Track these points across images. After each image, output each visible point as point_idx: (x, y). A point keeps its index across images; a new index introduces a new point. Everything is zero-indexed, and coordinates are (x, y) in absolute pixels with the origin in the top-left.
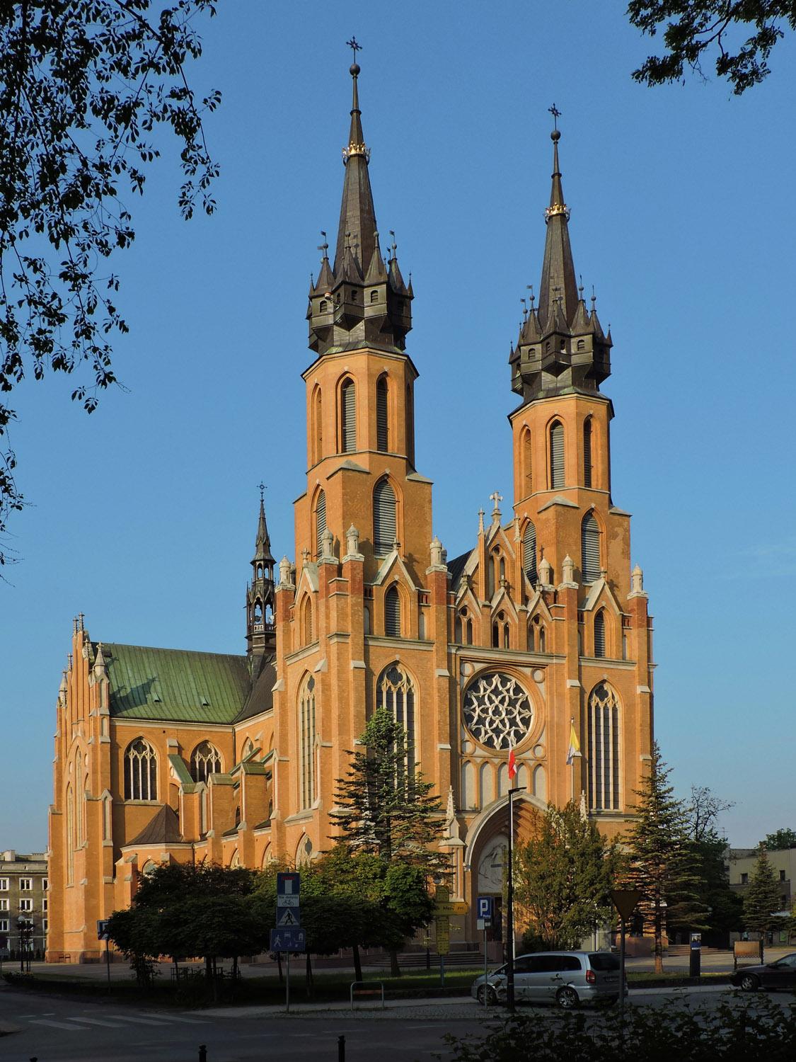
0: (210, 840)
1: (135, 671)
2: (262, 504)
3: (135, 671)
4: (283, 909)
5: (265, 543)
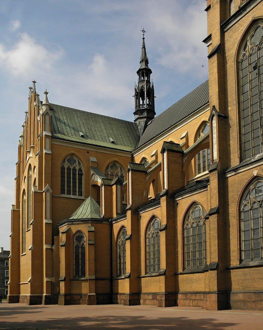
1: (69, 119)
2: (144, 41)
3: (69, 119)
5: (145, 61)
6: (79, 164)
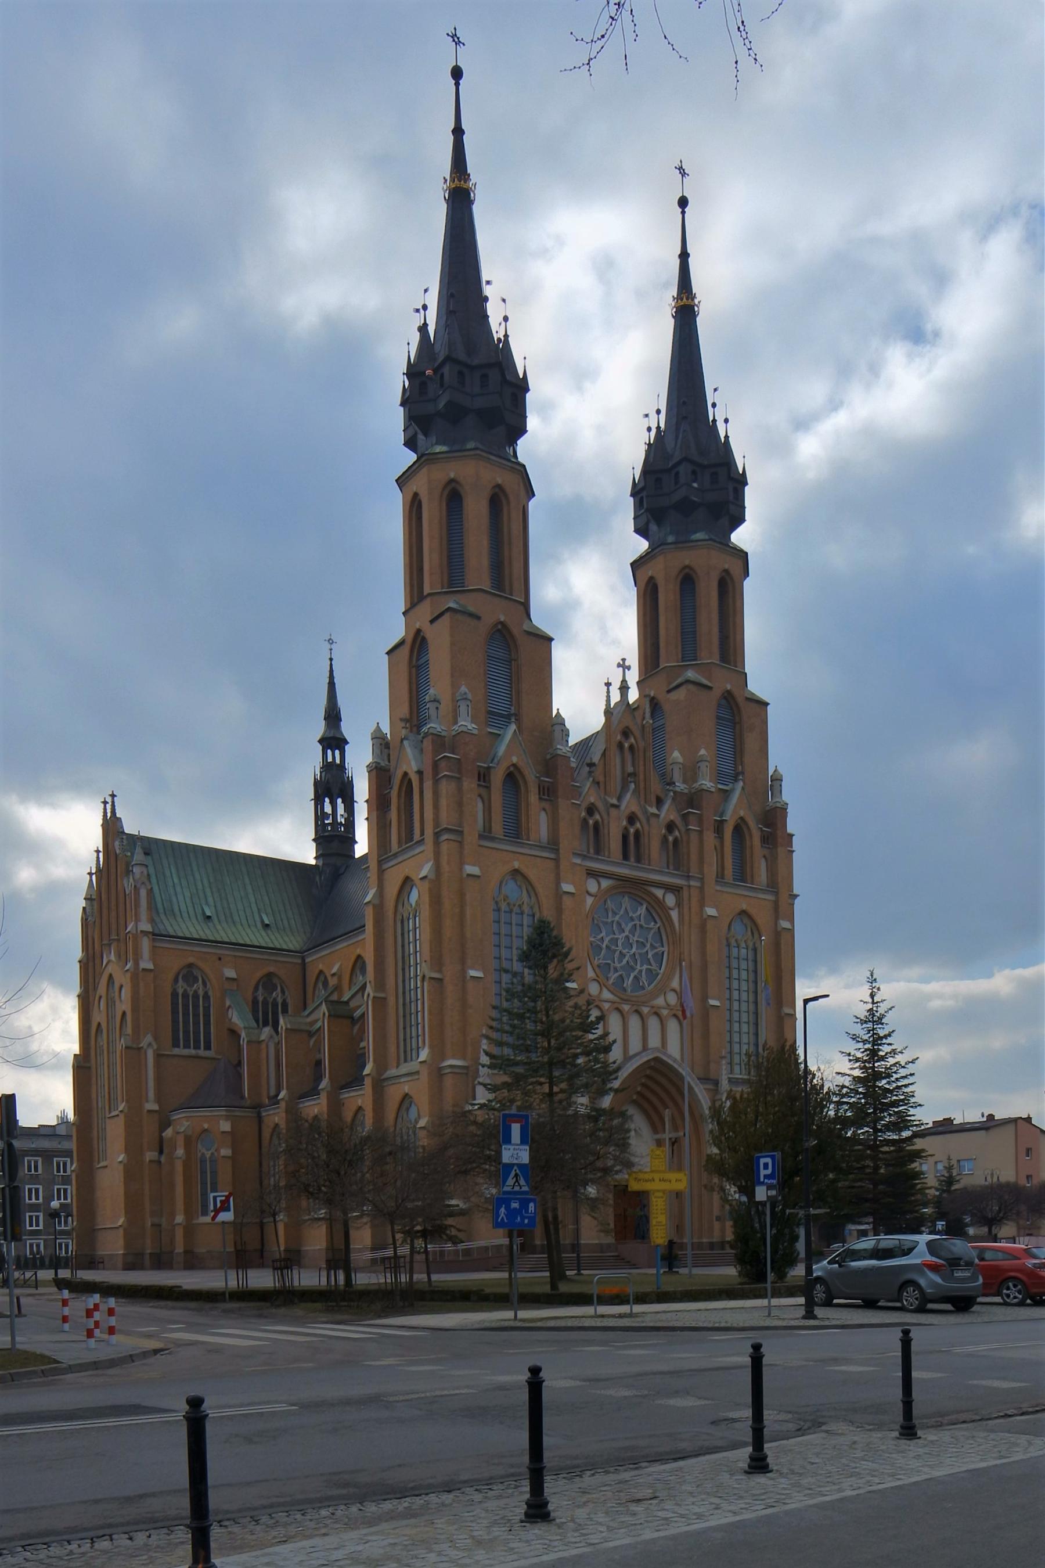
0: (283, 1104)
2: (608, 692)
4: (509, 1167)
5: (333, 716)
6: (283, 992)
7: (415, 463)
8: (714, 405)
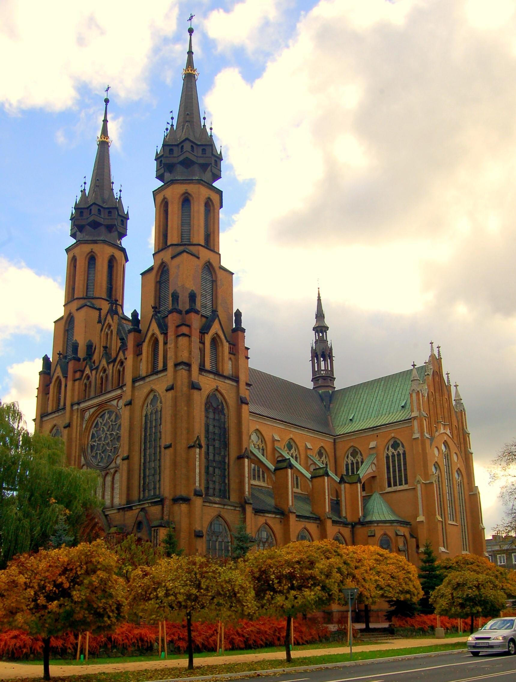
7: (75, 243)
8: (204, 118)
